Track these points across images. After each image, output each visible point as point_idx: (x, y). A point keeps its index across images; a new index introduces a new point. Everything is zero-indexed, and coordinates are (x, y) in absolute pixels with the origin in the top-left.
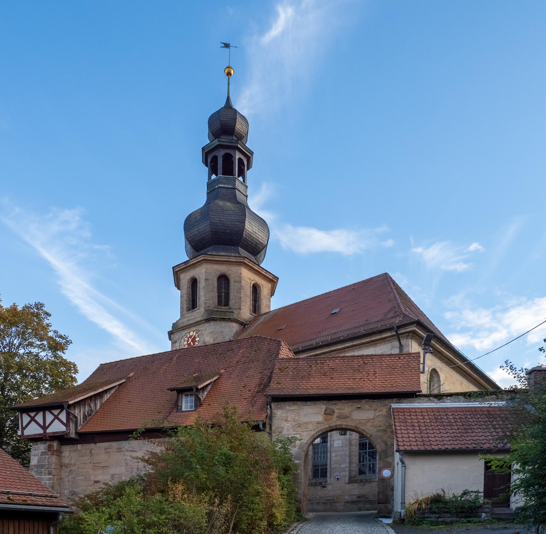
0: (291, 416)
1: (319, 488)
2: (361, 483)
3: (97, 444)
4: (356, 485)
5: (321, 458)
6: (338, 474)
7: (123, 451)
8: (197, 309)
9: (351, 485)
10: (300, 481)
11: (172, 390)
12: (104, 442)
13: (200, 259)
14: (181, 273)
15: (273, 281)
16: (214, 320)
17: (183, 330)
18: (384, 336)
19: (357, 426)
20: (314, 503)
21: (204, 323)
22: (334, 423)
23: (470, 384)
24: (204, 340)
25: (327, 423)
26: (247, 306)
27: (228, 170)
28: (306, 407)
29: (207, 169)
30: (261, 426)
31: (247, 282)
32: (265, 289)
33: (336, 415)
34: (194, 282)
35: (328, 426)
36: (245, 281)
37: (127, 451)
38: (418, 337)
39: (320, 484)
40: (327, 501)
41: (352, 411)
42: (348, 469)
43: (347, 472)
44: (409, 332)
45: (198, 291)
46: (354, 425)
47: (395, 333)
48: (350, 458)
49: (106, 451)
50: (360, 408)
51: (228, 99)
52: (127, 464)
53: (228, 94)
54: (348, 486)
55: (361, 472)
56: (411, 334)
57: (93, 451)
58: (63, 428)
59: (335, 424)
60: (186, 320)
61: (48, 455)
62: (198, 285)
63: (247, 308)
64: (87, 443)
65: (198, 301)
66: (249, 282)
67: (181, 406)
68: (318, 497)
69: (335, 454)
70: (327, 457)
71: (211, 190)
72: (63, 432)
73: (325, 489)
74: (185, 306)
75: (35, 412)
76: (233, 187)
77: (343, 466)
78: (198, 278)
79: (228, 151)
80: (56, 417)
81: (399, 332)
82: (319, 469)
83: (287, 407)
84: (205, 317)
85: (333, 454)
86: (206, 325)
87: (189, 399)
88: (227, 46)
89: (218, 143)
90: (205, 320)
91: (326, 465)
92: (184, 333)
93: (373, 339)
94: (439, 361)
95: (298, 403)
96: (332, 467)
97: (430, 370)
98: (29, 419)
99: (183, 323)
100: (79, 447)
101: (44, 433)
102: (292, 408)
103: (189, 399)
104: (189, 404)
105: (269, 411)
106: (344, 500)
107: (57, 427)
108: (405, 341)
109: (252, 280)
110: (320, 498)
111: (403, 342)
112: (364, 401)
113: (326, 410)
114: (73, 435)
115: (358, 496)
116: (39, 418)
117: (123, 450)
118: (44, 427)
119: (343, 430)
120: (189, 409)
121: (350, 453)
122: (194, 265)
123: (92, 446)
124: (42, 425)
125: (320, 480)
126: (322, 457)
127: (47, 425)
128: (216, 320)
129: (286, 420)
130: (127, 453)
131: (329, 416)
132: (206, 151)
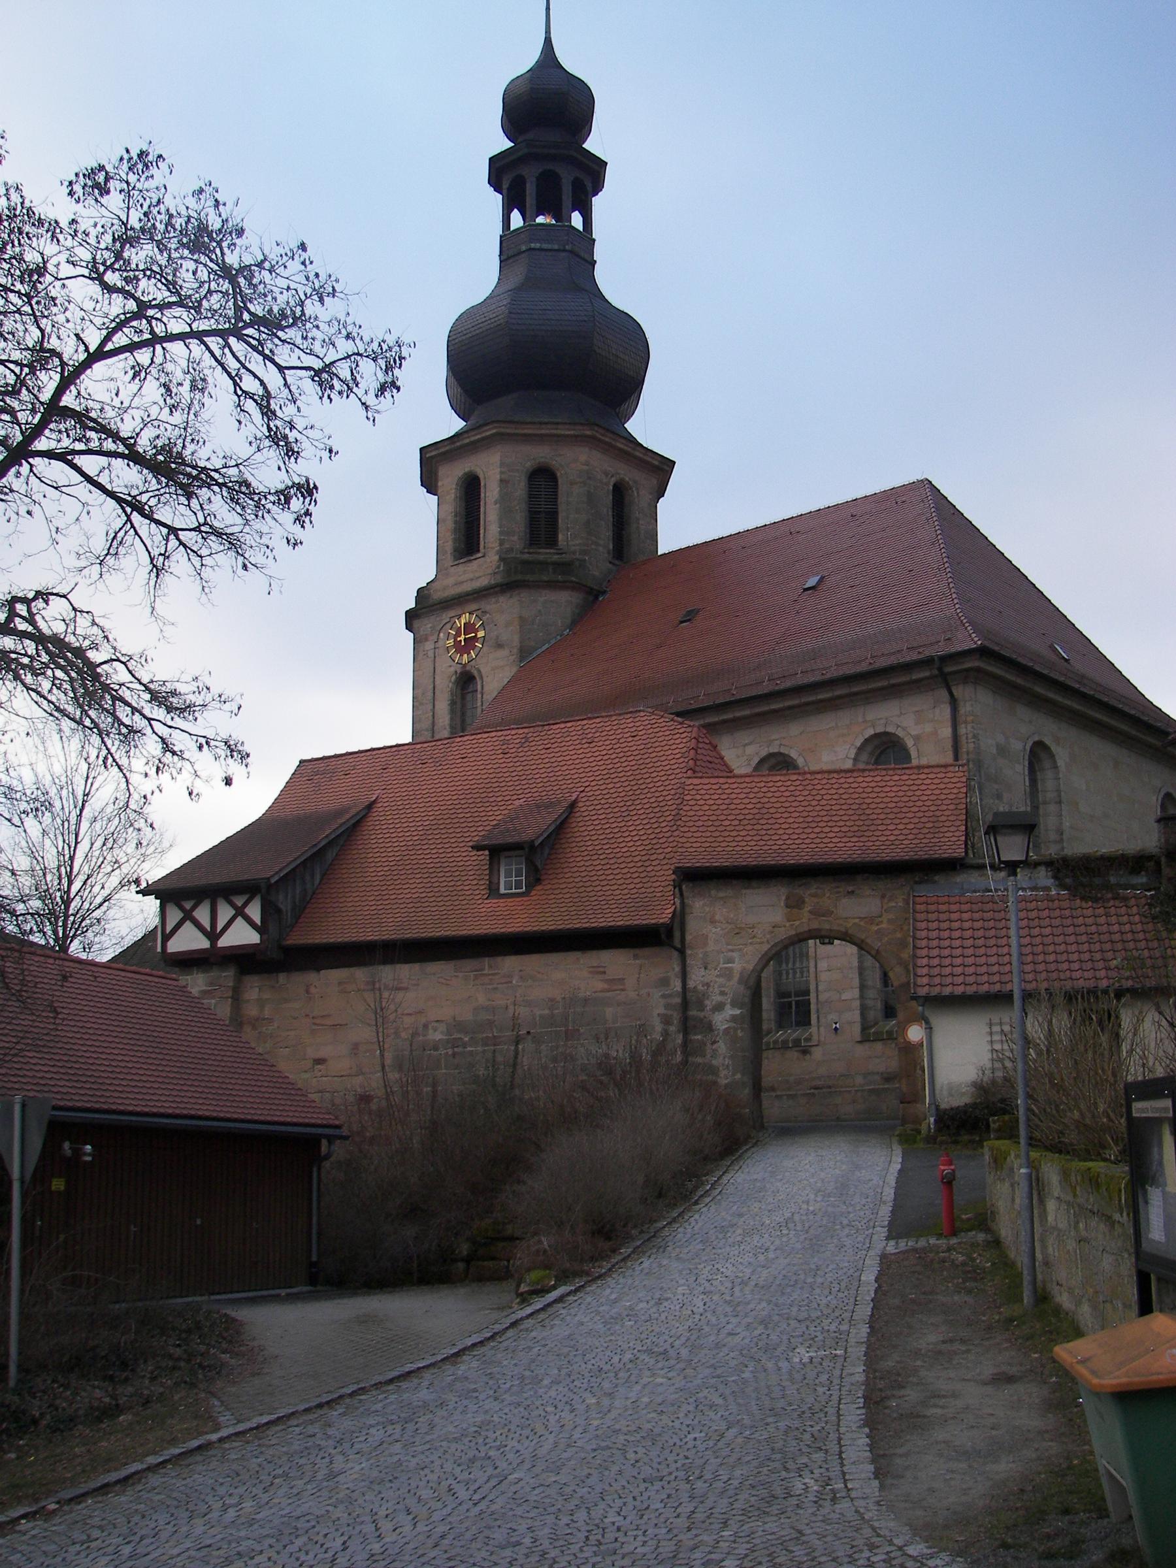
0: (721, 912)
1: (793, 1054)
2: (890, 1042)
4: (879, 1046)
9: (867, 1045)
11: (477, 848)
12: (337, 967)
13: (488, 433)
15: (662, 470)
18: (915, 676)
21: (496, 593)
24: (497, 637)
25: (792, 925)
26: (601, 542)
27: (550, 203)
28: (748, 891)
30: (663, 936)
33: (807, 908)
34: (471, 487)
35: (794, 933)
39: (797, 1043)
40: (812, 1091)
42: (857, 1003)
43: (858, 1012)
44: (967, 670)
45: (482, 509)
47: (936, 672)
50: (853, 892)
51: (548, 42)
54: (861, 1051)
57: (313, 990)
58: (253, 938)
59: (806, 929)
60: (450, 581)
61: (213, 998)
62: (482, 495)
63: (601, 549)
65: (482, 536)
66: (605, 480)
69: (826, 965)
71: (511, 253)
73: (808, 1057)
74: (449, 546)
75: (193, 899)
76: (562, 248)
78: (481, 477)
79: (550, 166)
80: (240, 912)
82: (790, 1003)
83: (713, 892)
84: (499, 579)
85: (823, 965)
87: (514, 867)
91: (807, 992)
92: (446, 616)
95: (735, 882)
96: (822, 997)
97: (1028, 748)
99: (444, 589)
100: (282, 977)
102: (721, 894)
103: (514, 867)
104: (514, 879)
105: (678, 901)
107: (241, 935)
108: (961, 687)
109: (612, 476)
111: (958, 691)
113: (788, 898)
116: (203, 914)
120: (514, 891)
123: (312, 977)
124: (209, 929)
125: (792, 1034)
129: (713, 922)
132: (497, 165)
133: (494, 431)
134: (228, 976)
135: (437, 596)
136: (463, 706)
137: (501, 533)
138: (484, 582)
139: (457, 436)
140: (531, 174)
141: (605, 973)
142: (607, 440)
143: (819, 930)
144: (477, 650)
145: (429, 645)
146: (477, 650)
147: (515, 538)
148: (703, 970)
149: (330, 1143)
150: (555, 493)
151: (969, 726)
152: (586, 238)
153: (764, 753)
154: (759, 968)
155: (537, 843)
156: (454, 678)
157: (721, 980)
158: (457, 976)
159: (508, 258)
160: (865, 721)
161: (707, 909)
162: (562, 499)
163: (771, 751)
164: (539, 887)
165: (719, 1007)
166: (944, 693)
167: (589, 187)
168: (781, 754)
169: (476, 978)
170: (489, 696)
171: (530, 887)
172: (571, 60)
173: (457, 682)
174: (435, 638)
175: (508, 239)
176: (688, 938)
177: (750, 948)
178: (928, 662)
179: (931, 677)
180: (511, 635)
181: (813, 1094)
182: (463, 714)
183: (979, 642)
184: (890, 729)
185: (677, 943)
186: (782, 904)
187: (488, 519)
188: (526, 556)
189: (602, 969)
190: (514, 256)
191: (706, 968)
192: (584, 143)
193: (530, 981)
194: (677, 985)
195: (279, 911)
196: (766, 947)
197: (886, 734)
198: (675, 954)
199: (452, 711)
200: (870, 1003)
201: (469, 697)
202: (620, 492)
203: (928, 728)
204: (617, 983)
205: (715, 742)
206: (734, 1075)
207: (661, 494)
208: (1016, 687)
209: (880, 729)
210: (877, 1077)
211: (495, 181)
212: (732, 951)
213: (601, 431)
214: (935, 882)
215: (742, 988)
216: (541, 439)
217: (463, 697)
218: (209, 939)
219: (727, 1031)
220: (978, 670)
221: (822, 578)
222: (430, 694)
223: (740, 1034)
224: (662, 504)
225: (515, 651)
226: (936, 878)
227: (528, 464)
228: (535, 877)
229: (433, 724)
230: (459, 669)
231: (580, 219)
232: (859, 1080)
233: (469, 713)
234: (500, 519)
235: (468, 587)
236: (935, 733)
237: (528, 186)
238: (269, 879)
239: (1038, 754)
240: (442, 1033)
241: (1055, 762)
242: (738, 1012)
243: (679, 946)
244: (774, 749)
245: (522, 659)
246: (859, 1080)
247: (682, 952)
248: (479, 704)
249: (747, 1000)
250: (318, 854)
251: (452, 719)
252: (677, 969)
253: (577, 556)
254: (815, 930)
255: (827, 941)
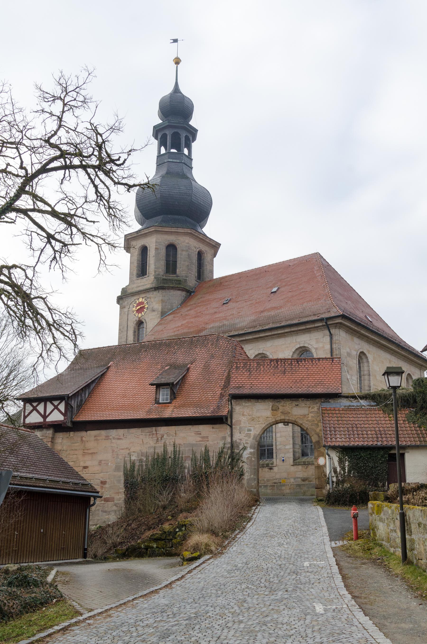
0: (247, 411)
1: (266, 469)
3: (88, 432)
4: (300, 467)
5: (267, 438)
6: (283, 455)
7: (111, 439)
8: (146, 276)
9: (295, 467)
10: (340, 543)
11: (152, 385)
13: (151, 230)
14: (132, 240)
15: (216, 247)
16: (162, 288)
17: (133, 296)
19: (296, 420)
20: (263, 487)
21: (153, 290)
22: (279, 417)
23: (399, 360)
26: (193, 273)
27: (176, 145)
28: (257, 404)
29: (157, 141)
30: (224, 420)
31: (193, 250)
32: (208, 255)
34: (144, 250)
36: (191, 249)
37: (114, 438)
38: (344, 327)
39: (267, 465)
41: (292, 408)
42: (291, 450)
45: (148, 259)
46: (294, 419)
47: (325, 324)
48: (293, 439)
49: (95, 438)
50: (298, 405)
52: (113, 451)
53: (177, 79)
54: (293, 469)
55: (304, 454)
56: (338, 325)
57: (84, 439)
59: (280, 419)
60: (135, 285)
62: (148, 254)
63: (193, 276)
64: (79, 431)
67: (159, 398)
68: (265, 480)
70: (272, 437)
71: (161, 163)
72: (61, 421)
74: (135, 273)
77: (287, 447)
78: (148, 247)
80: (56, 407)
81: (328, 323)
82: (265, 449)
83: (244, 404)
84: (154, 285)
85: (278, 435)
86: (155, 293)
88: (175, 41)
89: (168, 124)
90: (155, 288)
91: (272, 446)
92: (133, 299)
93: (308, 327)
94: (366, 344)
95: (252, 400)
96: (278, 448)
97: (358, 354)
98: (31, 408)
100: (72, 434)
101: (44, 421)
102: (247, 404)
105: (230, 407)
106: (290, 483)
110: (268, 481)
111: (333, 331)
112: (300, 400)
113: (272, 407)
114: (69, 425)
115: (302, 479)
116: (41, 408)
117: (110, 437)
118: (45, 417)
119: (286, 423)
120: (165, 402)
121: (293, 434)
122: (145, 235)
123: (83, 433)
124: (43, 414)
126: (268, 437)
127: (47, 414)
128: (165, 289)
129: (243, 415)
130: (114, 441)
131: (275, 412)
133: (154, 229)
134: (50, 432)
135: (129, 291)
136: (139, 333)
137: (155, 268)
138: (148, 286)
139: (139, 231)
140: (169, 133)
141: (201, 434)
142: (196, 234)
143: (285, 419)
144: (144, 312)
145: (126, 310)
146: (144, 312)
147: (160, 270)
148: (239, 434)
149: (95, 499)
150: (176, 254)
151: (337, 345)
152: (189, 157)
153: (257, 353)
154: (261, 434)
155: (175, 383)
156: (135, 323)
157: (246, 438)
158: (142, 434)
159: (160, 165)
160: (296, 342)
161: (241, 410)
162: (179, 256)
163: (259, 352)
164: (175, 400)
165: (245, 448)
166: (327, 332)
167: (191, 138)
168: (263, 353)
169: (150, 435)
170: (149, 330)
171: (172, 399)
172: (185, 90)
173: (137, 324)
174: (128, 307)
175: (160, 156)
176: (234, 421)
177: (258, 426)
178: (321, 320)
179: (323, 326)
180: (158, 306)
181: (274, 486)
182: (138, 336)
183: (341, 313)
184: (306, 345)
185: (229, 422)
186: (270, 409)
187: (150, 263)
188: (164, 277)
189: (199, 433)
190: (162, 164)
191: (240, 433)
192: (189, 122)
193: (171, 437)
194: (229, 440)
195: (72, 407)
196: (264, 426)
197: (304, 347)
198: (228, 427)
199: (134, 335)
200: (297, 450)
201: (141, 330)
202: (200, 254)
203: (321, 345)
204: (206, 438)
205: (243, 346)
206: (251, 475)
207: (215, 256)
208: (355, 331)
209: (302, 345)
210: (300, 480)
211: (155, 135)
212: (251, 427)
213: (195, 231)
214: (329, 402)
215: (254, 441)
216: (171, 233)
217: (139, 330)
218: (43, 418)
219: (248, 458)
220: (341, 323)
221: (279, 288)
222: (126, 328)
223: (253, 459)
224: (215, 259)
225: (160, 313)
226: (330, 400)
227: (166, 243)
228: (174, 396)
229: (127, 339)
230: (137, 319)
231: (187, 151)
232: (292, 480)
233: (140, 336)
234: (155, 263)
235: (141, 288)
236: (323, 347)
237: (168, 137)
238: (68, 395)
239: (362, 356)
240: (135, 457)
241: (368, 360)
242: (252, 450)
243: (230, 424)
244: (261, 352)
245: (162, 316)
246: (292, 480)
247: (231, 426)
248: (145, 332)
249: (256, 446)
250: (88, 386)
251: (134, 338)
252: (229, 433)
253: (184, 278)
254: (283, 419)
255: (286, 424)
